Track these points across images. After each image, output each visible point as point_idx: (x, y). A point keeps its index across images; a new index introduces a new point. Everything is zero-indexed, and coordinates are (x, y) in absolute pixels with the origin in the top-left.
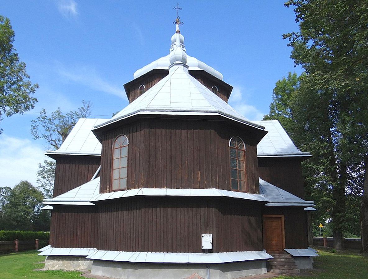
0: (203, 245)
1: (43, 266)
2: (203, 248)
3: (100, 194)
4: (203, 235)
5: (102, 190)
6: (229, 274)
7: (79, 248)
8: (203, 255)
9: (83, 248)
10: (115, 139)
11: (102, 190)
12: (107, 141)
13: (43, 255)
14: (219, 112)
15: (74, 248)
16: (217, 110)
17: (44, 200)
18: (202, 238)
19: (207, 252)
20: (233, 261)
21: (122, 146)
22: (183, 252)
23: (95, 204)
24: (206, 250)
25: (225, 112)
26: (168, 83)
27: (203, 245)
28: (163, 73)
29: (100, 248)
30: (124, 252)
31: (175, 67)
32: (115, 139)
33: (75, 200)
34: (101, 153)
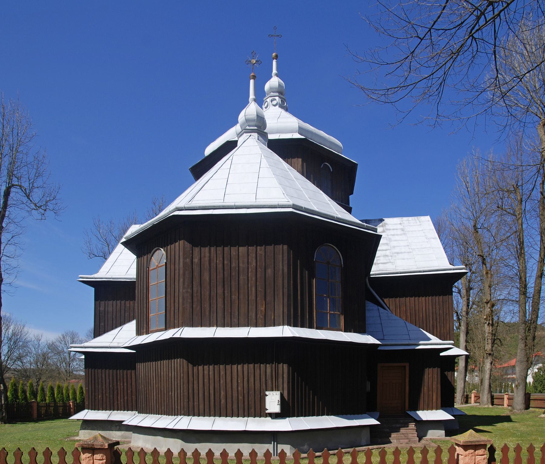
0: (267, 406)
1: (78, 435)
2: (267, 412)
3: (137, 337)
4: (267, 393)
5: (139, 332)
6: (306, 446)
7: (122, 411)
8: (97, 413)
9: (128, 411)
10: (151, 254)
11: (139, 332)
12: (142, 258)
13: (78, 420)
14: (294, 207)
15: (115, 411)
16: (291, 203)
17: (277, 364)
18: (267, 398)
19: (101, 409)
20: (310, 428)
21: (159, 265)
22: (241, 417)
23: (135, 351)
24: (273, 413)
25: (335, 215)
26: (229, 162)
27: (267, 407)
28: (230, 146)
29: (141, 411)
30: (165, 416)
31: (245, 136)
32: (151, 254)
33: (112, 345)
34: (135, 277)
